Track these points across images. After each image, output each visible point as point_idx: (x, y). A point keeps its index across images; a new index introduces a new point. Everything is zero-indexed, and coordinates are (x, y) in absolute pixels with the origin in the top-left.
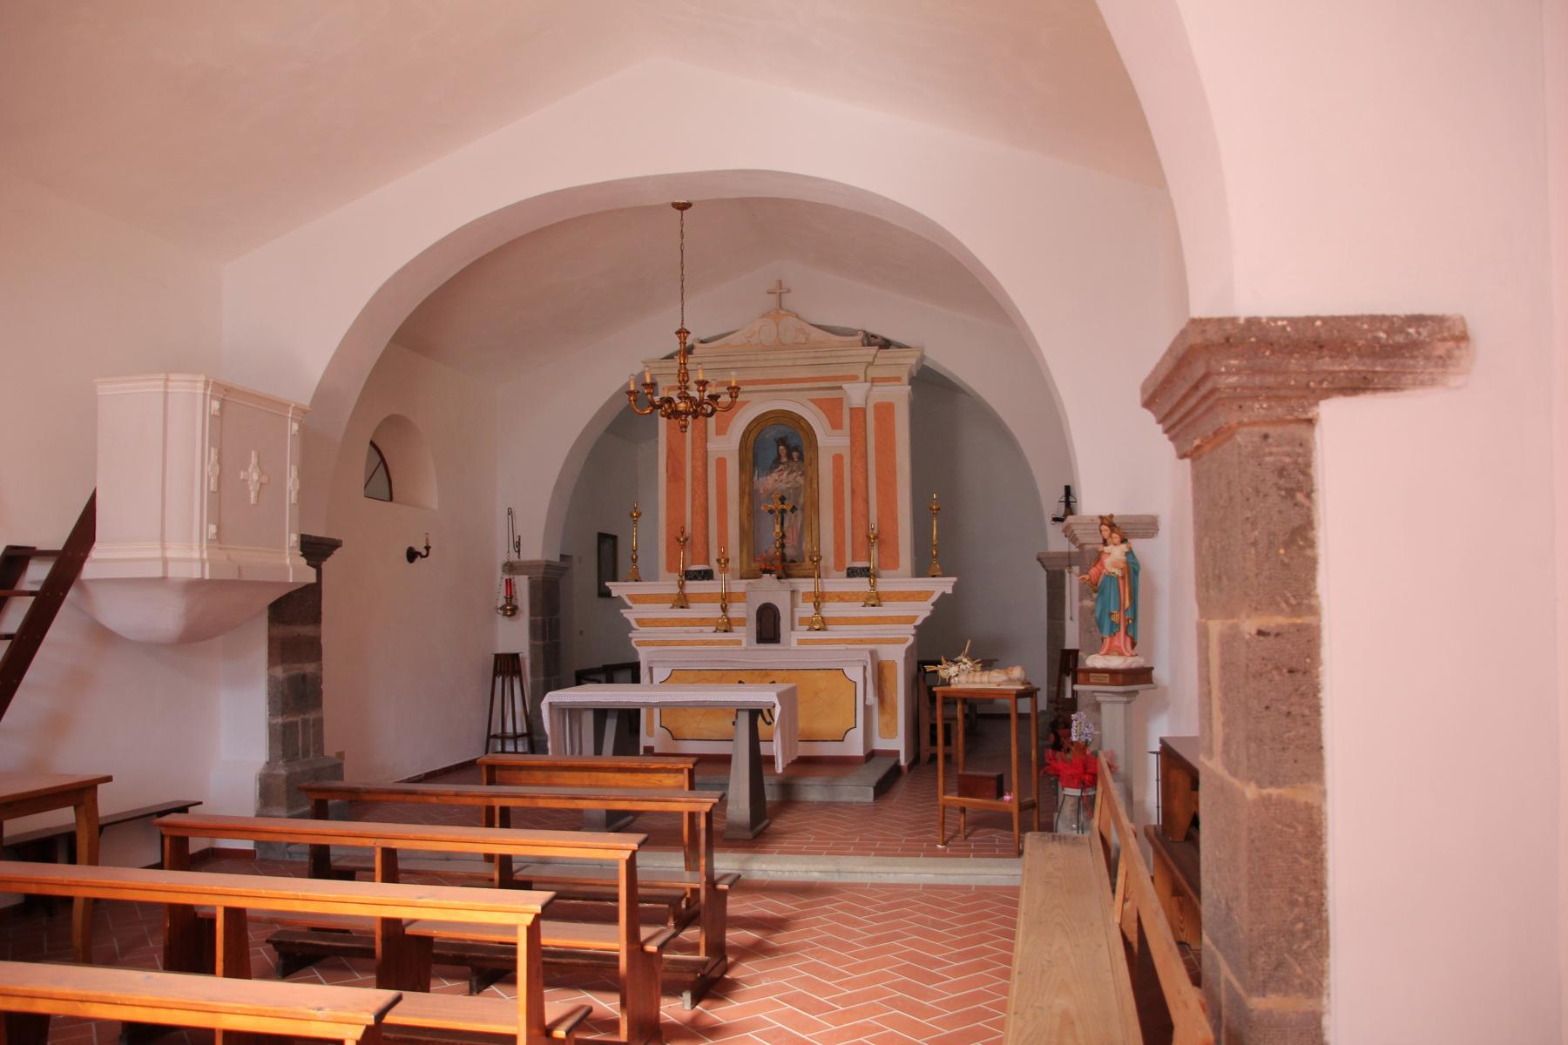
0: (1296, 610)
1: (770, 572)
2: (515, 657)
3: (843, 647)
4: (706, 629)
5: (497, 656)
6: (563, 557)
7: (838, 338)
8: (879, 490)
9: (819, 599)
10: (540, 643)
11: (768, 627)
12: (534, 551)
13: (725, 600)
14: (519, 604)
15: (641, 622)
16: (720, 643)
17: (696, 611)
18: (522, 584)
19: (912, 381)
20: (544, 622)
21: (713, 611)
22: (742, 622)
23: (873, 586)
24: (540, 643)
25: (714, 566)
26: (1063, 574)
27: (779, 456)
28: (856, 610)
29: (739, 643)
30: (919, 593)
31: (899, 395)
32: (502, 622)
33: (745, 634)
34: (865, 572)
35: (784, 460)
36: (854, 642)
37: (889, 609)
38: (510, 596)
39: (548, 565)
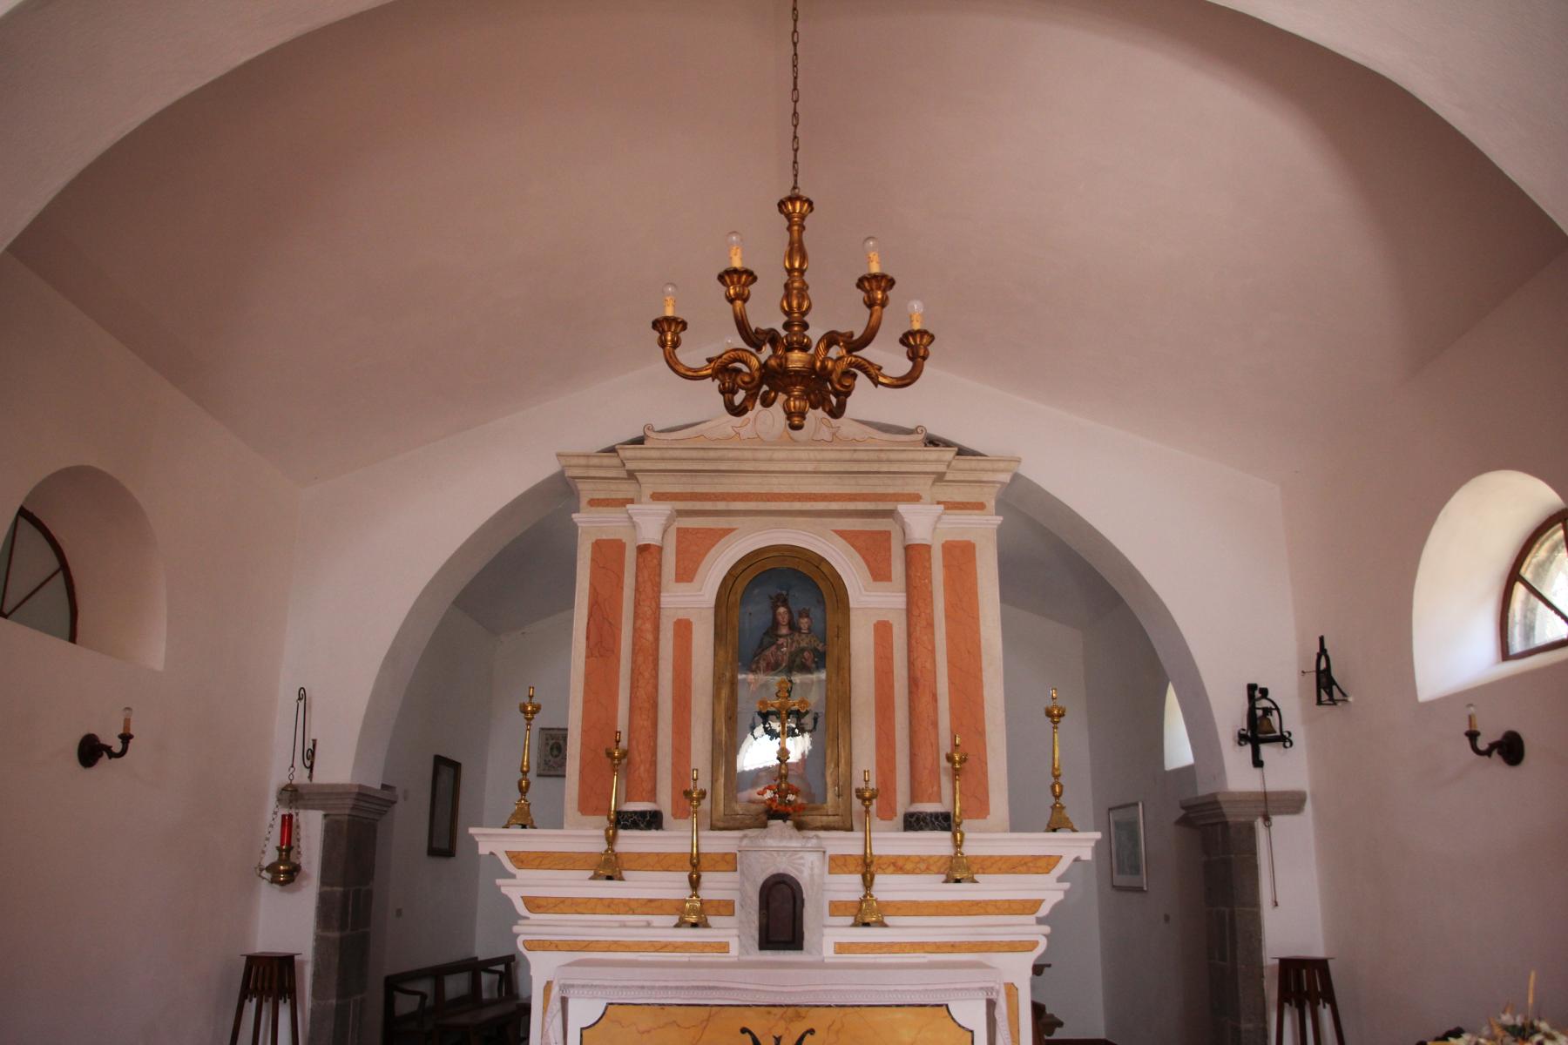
1: (784, 817)
2: (286, 963)
4: (657, 920)
5: (252, 961)
6: (384, 787)
7: (887, 436)
8: (951, 682)
9: (867, 868)
10: (335, 935)
11: (781, 918)
12: (339, 767)
13: (695, 866)
14: (303, 861)
15: (533, 904)
17: (637, 885)
18: (312, 825)
19: (1003, 506)
20: (345, 895)
21: (673, 886)
22: (726, 908)
23: (958, 845)
24: (335, 935)
25: (664, 802)
26: (1251, 830)
27: (775, 624)
28: (931, 888)
29: (723, 948)
30: (1036, 858)
31: (982, 530)
32: (269, 896)
33: (735, 934)
34: (943, 822)
35: (784, 631)
37: (990, 887)
38: (288, 844)
39: (362, 795)
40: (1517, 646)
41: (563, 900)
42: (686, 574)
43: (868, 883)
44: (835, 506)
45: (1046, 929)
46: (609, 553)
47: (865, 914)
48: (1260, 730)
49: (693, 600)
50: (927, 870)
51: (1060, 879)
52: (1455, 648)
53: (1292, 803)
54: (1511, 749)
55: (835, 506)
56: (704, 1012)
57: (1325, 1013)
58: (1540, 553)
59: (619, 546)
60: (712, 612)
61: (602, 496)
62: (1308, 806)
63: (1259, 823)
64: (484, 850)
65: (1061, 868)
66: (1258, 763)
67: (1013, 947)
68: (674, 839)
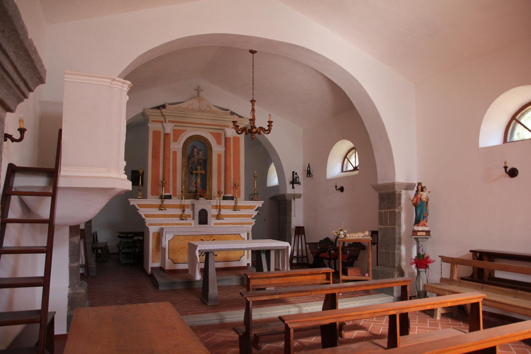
0: (381, 212)
1: (203, 197)
3: (183, 226)
4: (174, 219)
7: (222, 111)
11: (203, 218)
13: (183, 207)
15: (146, 216)
16: (181, 224)
26: (291, 201)
28: (231, 212)
29: (191, 224)
34: (232, 198)
36: (237, 224)
37: (243, 212)
40: (344, 170)
41: (153, 215)
42: (175, 140)
43: (220, 211)
44: (210, 127)
45: (255, 220)
46: (156, 134)
47: (218, 217)
48: (295, 181)
49: (177, 147)
50: (229, 208)
51: (256, 210)
52: (334, 169)
53: (299, 196)
54: (342, 189)
55: (210, 127)
56: (193, 236)
57: (303, 236)
58: (350, 153)
59: (159, 133)
60: (181, 150)
61: (155, 119)
62: (302, 197)
63: (293, 200)
64: (131, 204)
65: (256, 208)
66: (293, 188)
67: (248, 224)
68: (175, 201)
